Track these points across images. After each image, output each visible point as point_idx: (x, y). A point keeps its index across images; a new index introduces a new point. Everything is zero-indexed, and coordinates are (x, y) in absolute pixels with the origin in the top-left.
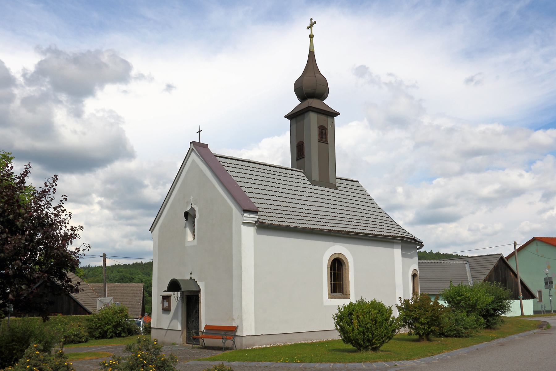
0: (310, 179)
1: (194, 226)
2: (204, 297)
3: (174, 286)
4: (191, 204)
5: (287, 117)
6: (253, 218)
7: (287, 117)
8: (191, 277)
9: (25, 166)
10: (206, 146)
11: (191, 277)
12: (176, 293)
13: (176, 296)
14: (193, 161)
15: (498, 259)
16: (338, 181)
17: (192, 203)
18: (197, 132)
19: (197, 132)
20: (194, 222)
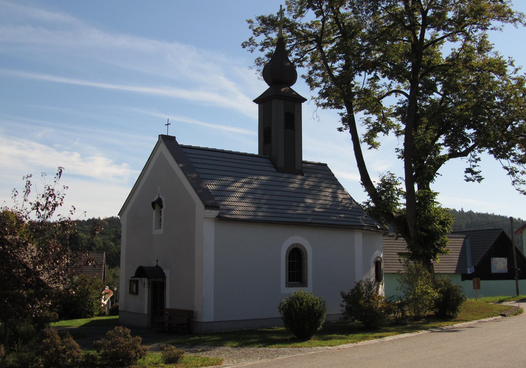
0: (276, 167)
1: (161, 215)
2: (255, 349)
3: (141, 272)
4: (159, 194)
5: (256, 101)
6: (215, 213)
7: (256, 101)
8: (157, 264)
9: (71, 211)
10: (173, 138)
11: (157, 264)
12: (143, 279)
13: (143, 282)
14: (161, 153)
15: (499, 234)
16: (304, 165)
17: (160, 194)
18: (166, 125)
19: (166, 125)
20: (161, 212)
